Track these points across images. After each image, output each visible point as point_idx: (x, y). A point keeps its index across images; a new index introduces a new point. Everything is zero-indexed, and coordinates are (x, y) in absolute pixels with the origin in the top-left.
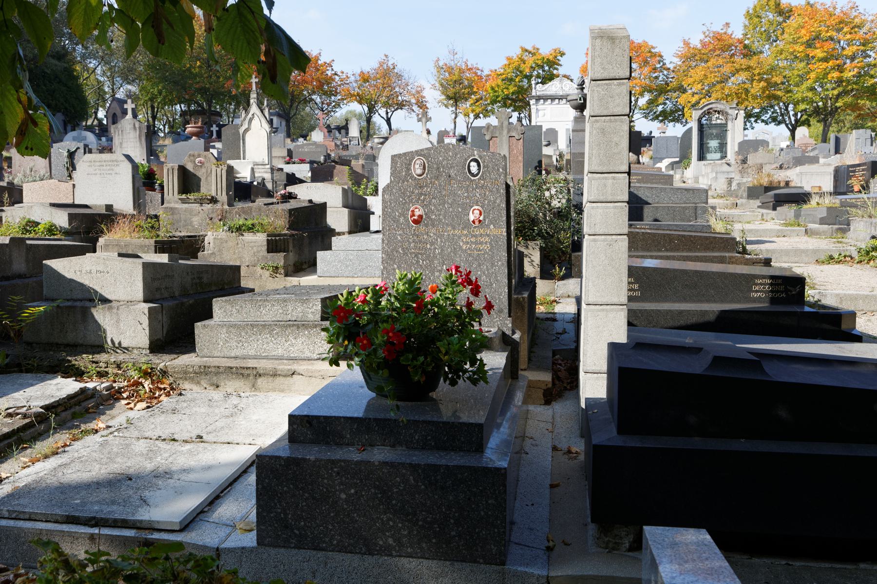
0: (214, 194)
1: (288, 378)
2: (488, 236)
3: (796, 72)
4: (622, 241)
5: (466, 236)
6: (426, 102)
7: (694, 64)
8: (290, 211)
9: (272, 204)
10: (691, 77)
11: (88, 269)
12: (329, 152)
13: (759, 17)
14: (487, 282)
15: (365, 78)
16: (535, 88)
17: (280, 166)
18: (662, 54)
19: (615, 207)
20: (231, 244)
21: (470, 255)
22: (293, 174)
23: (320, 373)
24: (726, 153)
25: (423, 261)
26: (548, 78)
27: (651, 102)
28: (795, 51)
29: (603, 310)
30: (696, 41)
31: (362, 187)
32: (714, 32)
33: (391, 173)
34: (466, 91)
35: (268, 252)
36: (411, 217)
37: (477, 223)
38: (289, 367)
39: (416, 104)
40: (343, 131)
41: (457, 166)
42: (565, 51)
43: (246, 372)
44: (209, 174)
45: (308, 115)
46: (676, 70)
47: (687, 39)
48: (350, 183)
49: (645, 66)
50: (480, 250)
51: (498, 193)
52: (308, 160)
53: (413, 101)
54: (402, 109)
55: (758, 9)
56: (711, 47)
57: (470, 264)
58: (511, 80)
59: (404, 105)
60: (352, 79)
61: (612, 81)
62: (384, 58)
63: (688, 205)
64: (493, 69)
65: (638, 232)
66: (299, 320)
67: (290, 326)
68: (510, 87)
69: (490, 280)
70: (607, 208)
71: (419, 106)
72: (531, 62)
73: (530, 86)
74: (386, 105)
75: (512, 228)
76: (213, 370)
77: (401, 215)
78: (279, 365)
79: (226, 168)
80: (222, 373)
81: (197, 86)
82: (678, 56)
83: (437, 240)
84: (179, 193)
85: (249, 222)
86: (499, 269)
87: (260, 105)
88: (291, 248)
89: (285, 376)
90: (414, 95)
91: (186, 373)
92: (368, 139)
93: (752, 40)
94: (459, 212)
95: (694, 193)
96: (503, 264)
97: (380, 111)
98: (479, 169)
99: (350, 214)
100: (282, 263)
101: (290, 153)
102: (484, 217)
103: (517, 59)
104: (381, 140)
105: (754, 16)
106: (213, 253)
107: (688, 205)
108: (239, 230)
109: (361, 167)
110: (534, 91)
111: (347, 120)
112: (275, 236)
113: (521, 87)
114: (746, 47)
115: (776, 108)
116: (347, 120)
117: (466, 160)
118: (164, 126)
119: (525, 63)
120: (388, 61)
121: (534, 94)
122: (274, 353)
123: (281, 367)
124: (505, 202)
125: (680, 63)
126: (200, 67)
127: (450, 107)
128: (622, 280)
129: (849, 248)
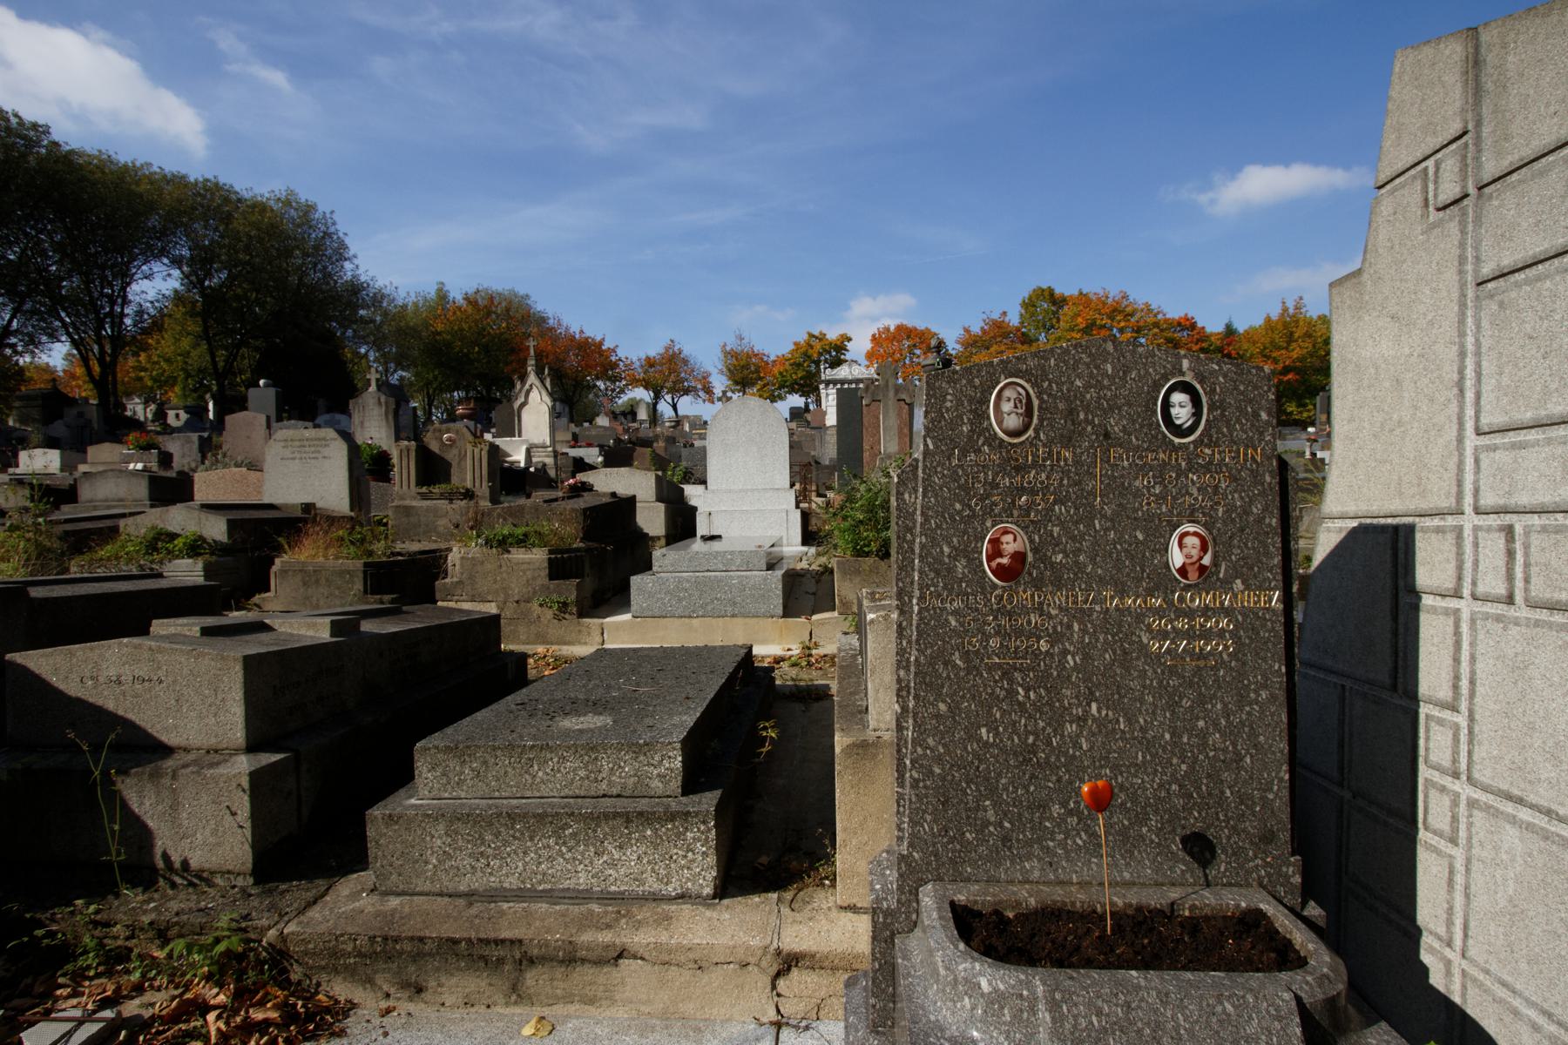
0: (469, 484)
2: (1228, 612)
9: (556, 500)
11: (113, 672)
13: (1034, 306)
14: (1225, 750)
15: (650, 363)
17: (565, 450)
20: (489, 566)
21: (1172, 671)
22: (581, 459)
23: (691, 956)
25: (1027, 690)
26: (836, 363)
30: (976, 329)
34: (754, 376)
35: (551, 579)
36: (989, 559)
37: (1193, 575)
39: (702, 390)
40: (629, 417)
41: (1130, 405)
43: (495, 953)
44: (463, 457)
47: (966, 326)
53: (699, 386)
56: (992, 334)
57: (1171, 697)
58: (799, 365)
66: (628, 793)
67: (607, 816)
69: (1234, 744)
74: (673, 391)
76: (407, 946)
77: (957, 553)
79: (487, 448)
80: (430, 954)
83: (1070, 627)
84: (417, 484)
85: (519, 531)
86: (1262, 712)
88: (587, 570)
89: (599, 962)
91: (335, 954)
94: (1138, 542)
96: (1273, 697)
98: (1197, 414)
100: (573, 597)
101: (575, 437)
102: (1215, 557)
104: (673, 424)
105: (1029, 305)
106: (460, 582)
110: (823, 375)
111: (632, 406)
112: (562, 552)
113: (809, 372)
114: (1023, 334)
117: (1157, 387)
118: (442, 414)
122: (566, 884)
123: (586, 937)
126: (478, 352)
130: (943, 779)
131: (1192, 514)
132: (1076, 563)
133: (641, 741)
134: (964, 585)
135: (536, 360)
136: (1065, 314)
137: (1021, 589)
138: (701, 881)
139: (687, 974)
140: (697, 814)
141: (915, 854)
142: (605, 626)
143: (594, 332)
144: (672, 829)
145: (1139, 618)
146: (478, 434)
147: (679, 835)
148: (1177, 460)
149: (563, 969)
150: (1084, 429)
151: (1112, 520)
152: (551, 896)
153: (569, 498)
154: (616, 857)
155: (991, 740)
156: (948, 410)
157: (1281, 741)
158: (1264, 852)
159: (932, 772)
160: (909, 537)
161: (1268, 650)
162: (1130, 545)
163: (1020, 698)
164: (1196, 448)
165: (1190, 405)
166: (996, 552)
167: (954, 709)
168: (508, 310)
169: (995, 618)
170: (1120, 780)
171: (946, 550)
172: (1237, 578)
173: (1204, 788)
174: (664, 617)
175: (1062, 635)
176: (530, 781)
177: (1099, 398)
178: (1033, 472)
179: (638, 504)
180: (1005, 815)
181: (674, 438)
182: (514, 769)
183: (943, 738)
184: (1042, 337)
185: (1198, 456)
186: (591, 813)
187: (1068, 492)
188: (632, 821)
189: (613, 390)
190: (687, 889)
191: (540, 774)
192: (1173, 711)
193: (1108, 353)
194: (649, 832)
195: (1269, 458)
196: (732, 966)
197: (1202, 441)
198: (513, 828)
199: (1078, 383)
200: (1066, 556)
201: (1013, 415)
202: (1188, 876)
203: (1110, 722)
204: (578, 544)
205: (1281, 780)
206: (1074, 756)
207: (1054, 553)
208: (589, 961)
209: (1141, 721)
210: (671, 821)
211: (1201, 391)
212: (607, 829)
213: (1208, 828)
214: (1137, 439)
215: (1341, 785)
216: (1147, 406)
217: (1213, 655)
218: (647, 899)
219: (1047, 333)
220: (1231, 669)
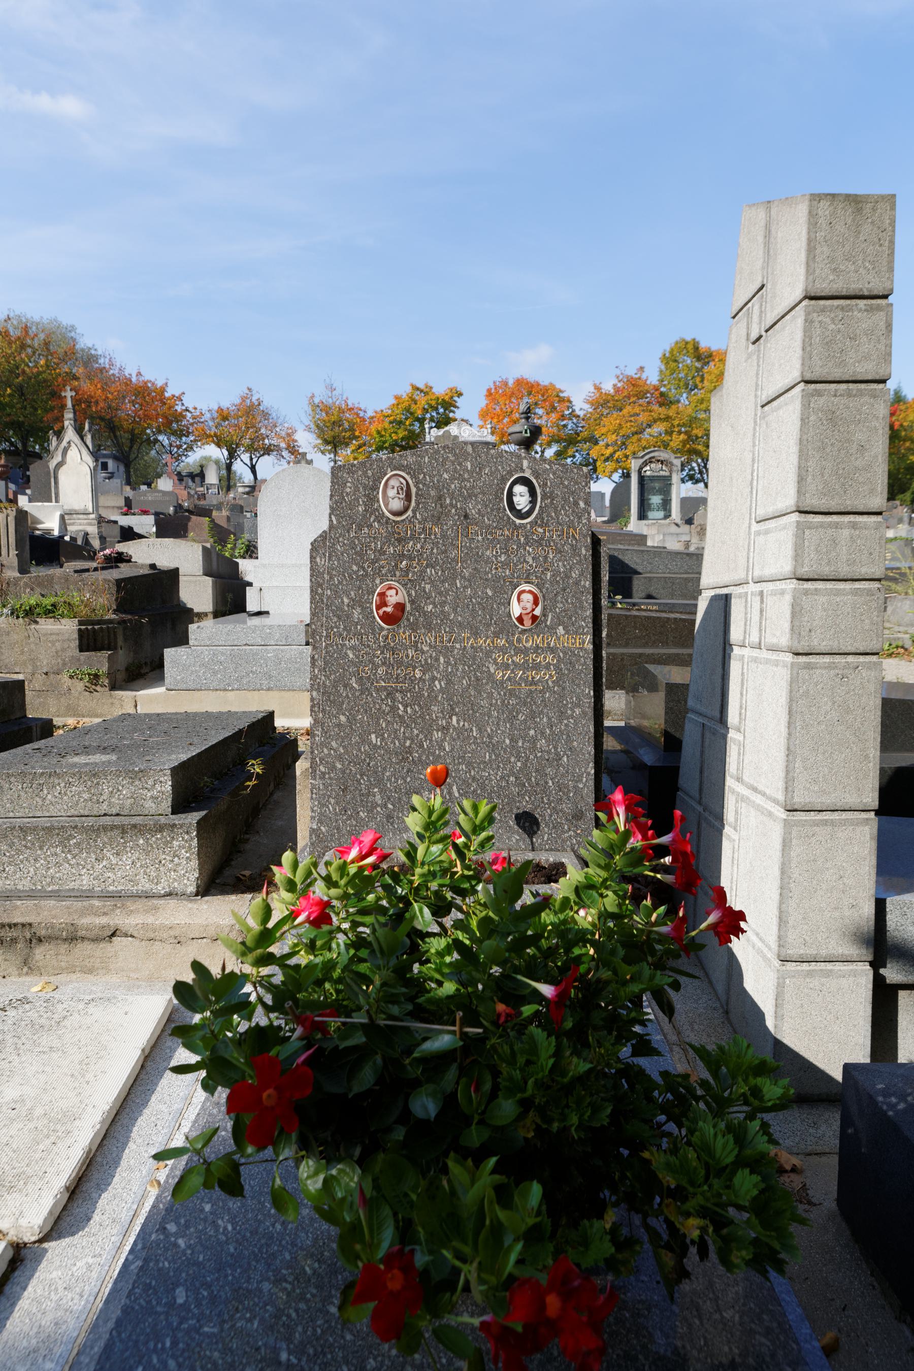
1: (102, 945)
2: (553, 650)
4: (869, 668)
5: (503, 650)
7: (607, 411)
8: (118, 582)
9: (87, 570)
12: (180, 502)
13: (676, 361)
14: (549, 752)
15: (224, 416)
17: (113, 518)
18: (572, 399)
19: (855, 592)
20: (16, 637)
21: (511, 693)
23: (172, 933)
24: (670, 511)
25: (406, 706)
27: (558, 454)
29: (825, 823)
30: (608, 387)
31: (229, 546)
32: (627, 377)
33: (331, 508)
34: (348, 434)
35: (81, 651)
37: (528, 622)
38: (104, 920)
40: (197, 479)
41: (484, 494)
42: (462, 391)
45: (154, 460)
47: (597, 383)
48: (212, 540)
49: (552, 412)
51: (574, 555)
52: (153, 511)
53: (283, 445)
56: (626, 394)
57: (510, 712)
58: (400, 423)
59: (272, 451)
60: (207, 416)
61: (854, 302)
62: (247, 392)
63: (636, 548)
64: (378, 410)
65: (668, 618)
66: (126, 812)
67: (105, 828)
68: (399, 431)
69: (555, 748)
70: (838, 593)
71: (290, 452)
72: (423, 402)
74: (251, 449)
75: (604, 634)
77: (354, 602)
78: (83, 913)
79: (14, 513)
81: (8, 419)
82: (588, 402)
83: (437, 660)
85: (48, 602)
86: (576, 724)
87: (79, 431)
88: (120, 642)
89: (96, 940)
90: (284, 438)
92: (229, 488)
94: (488, 597)
96: (584, 713)
97: (242, 456)
98: (533, 502)
99: (215, 585)
100: (104, 669)
101: (128, 503)
102: (544, 609)
103: (407, 398)
104: (247, 489)
105: (670, 360)
108: (31, 614)
109: (225, 520)
110: (427, 436)
111: (202, 467)
112: (93, 623)
113: (412, 432)
114: (662, 394)
115: (694, 465)
116: (202, 467)
117: (504, 480)
121: (427, 440)
122: (72, 885)
123: (85, 921)
124: (589, 577)
125: (590, 410)
128: (867, 757)
129: (899, 635)
130: (343, 772)
131: (528, 577)
132: (442, 612)
133: (137, 769)
134: (359, 627)
135: (75, 413)
136: (710, 373)
137: (401, 631)
138: (185, 881)
139: (168, 948)
140: (181, 826)
141: (322, 828)
142: (138, 699)
143: (154, 375)
144: (161, 839)
145: (488, 654)
146: (11, 496)
147: (166, 843)
148: (517, 536)
149: (66, 946)
150: (450, 511)
151: (469, 581)
152: (57, 895)
153: (103, 568)
154: (114, 862)
155: (379, 743)
156: (348, 494)
157: (589, 745)
158: (576, 826)
159: (334, 767)
160: (320, 591)
161: (581, 679)
162: (482, 599)
163: (401, 713)
164: (532, 527)
165: (528, 495)
166: (383, 603)
167: (351, 720)
168: (47, 344)
169: (382, 653)
170: (472, 773)
171: (346, 600)
172: (559, 625)
173: (533, 779)
174: (198, 690)
175: (432, 666)
176: (40, 803)
177: (461, 488)
178: (411, 543)
179: (181, 578)
180: (389, 799)
181: (242, 507)
182: (26, 793)
183: (343, 742)
184: (684, 399)
185: (533, 533)
186: (92, 826)
187: (436, 558)
188: (127, 832)
189: (179, 447)
190: (174, 888)
191: (49, 797)
192: (512, 723)
193: (468, 454)
194: (141, 841)
195: (585, 536)
196: (205, 940)
197: (537, 522)
198: (25, 839)
199: (446, 476)
200: (435, 607)
201: (396, 499)
202: (521, 843)
203: (466, 730)
204: (111, 616)
205: (589, 774)
206: (439, 756)
207: (426, 604)
208: (89, 939)
209: (489, 730)
210: (160, 832)
211: (536, 485)
212: (106, 840)
213: (536, 808)
214: (489, 520)
215: (700, 803)
216: (496, 495)
217: (541, 682)
218: (140, 897)
219: (689, 393)
220: (554, 692)
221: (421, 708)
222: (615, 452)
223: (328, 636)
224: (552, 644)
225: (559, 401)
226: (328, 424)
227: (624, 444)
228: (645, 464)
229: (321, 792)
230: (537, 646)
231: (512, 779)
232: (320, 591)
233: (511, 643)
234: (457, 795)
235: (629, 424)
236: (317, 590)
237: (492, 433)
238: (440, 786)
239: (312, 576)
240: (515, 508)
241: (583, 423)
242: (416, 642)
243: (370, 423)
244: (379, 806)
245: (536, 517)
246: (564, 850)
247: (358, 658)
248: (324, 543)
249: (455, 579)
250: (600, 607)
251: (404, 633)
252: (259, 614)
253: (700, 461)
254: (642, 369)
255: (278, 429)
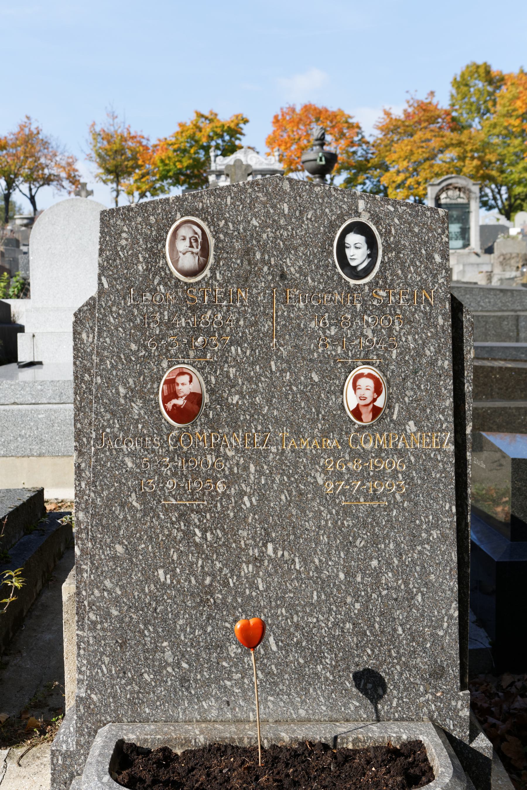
2: (401, 453)
3: (511, 150)
5: (334, 454)
6: (79, 176)
10: (395, 152)
13: (467, 85)
16: (215, 161)
21: (346, 511)
24: (469, 240)
25: (204, 532)
28: (510, 125)
30: (398, 112)
32: (418, 101)
34: (130, 163)
36: (166, 400)
37: (367, 416)
39: (67, 179)
41: (306, 245)
42: (249, 118)
46: (376, 144)
47: (387, 108)
49: (341, 138)
50: (375, 497)
51: (428, 326)
53: (63, 175)
54: (49, 184)
55: (466, 77)
56: (416, 119)
57: (345, 537)
58: (184, 151)
59: (52, 181)
62: (26, 120)
63: (506, 314)
64: (162, 137)
65: (492, 368)
68: (184, 160)
69: (406, 584)
71: (70, 182)
72: (208, 130)
73: (208, 158)
74: (30, 179)
75: (469, 430)
82: (378, 128)
83: (246, 468)
86: (433, 550)
90: (64, 168)
93: (460, 111)
94: (313, 384)
95: (512, 296)
96: (444, 537)
97: (21, 187)
98: (373, 255)
102: (389, 398)
103: (191, 126)
104: (25, 221)
107: (506, 314)
113: (197, 161)
114: (454, 119)
117: (333, 227)
119: (200, 131)
120: (30, 124)
125: (380, 136)
127: (109, 183)
130: (121, 621)
131: (366, 356)
132: (253, 404)
134: (140, 426)
136: (502, 97)
137: (197, 430)
141: (93, 696)
148: (352, 302)
150: (261, 269)
151: (288, 362)
155: (169, 581)
158: (435, 687)
159: (109, 614)
160: (87, 377)
162: (306, 386)
163: (197, 540)
165: (365, 246)
169: (172, 460)
170: (295, 620)
171: (122, 391)
172: (410, 419)
173: (377, 626)
177: (276, 238)
178: (209, 313)
180: (183, 656)
183: (120, 580)
184: (476, 123)
187: (243, 333)
192: (348, 552)
193: (285, 193)
195: (442, 301)
197: (377, 283)
199: (254, 222)
200: (243, 397)
201: (189, 255)
202: (361, 712)
203: (286, 562)
205: (451, 617)
206: (250, 597)
207: (230, 394)
209: (317, 561)
213: (381, 665)
214: (313, 280)
216: (323, 247)
219: (481, 118)
220: (404, 509)
221: (225, 534)
222: (406, 179)
223: (98, 439)
224: (400, 445)
225: (348, 128)
226: (110, 153)
227: (415, 170)
228: (442, 190)
229: (91, 648)
230: (380, 447)
231: (348, 625)
232: (87, 377)
233: (344, 445)
234: (274, 648)
235: (420, 150)
236: (83, 377)
237: (280, 161)
238: (254, 648)
239: (76, 357)
240: (348, 264)
241: (373, 150)
242: (218, 445)
243: (153, 151)
244: (169, 665)
245: (376, 276)
246: (420, 719)
247: (139, 467)
248: (92, 314)
249: (268, 360)
250: (463, 394)
251: (201, 433)
252: (31, 364)
253: (493, 186)
254: (432, 93)
255: (58, 159)
